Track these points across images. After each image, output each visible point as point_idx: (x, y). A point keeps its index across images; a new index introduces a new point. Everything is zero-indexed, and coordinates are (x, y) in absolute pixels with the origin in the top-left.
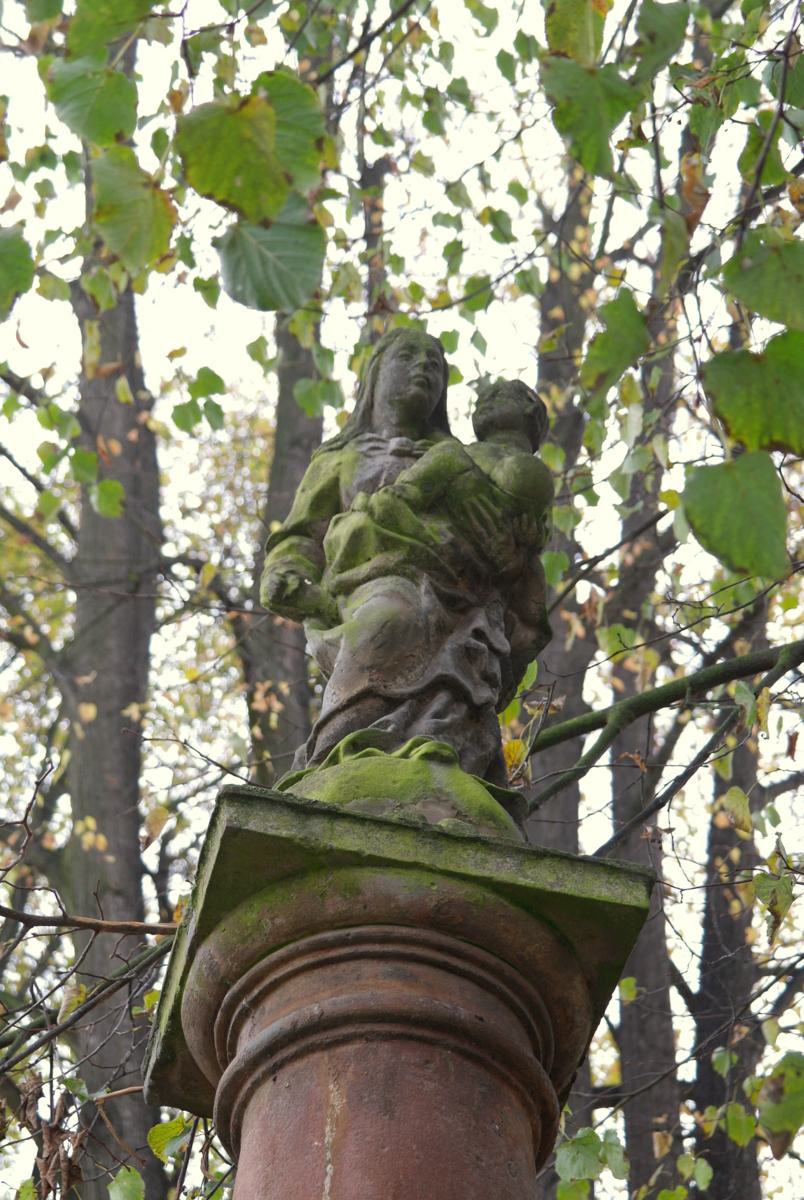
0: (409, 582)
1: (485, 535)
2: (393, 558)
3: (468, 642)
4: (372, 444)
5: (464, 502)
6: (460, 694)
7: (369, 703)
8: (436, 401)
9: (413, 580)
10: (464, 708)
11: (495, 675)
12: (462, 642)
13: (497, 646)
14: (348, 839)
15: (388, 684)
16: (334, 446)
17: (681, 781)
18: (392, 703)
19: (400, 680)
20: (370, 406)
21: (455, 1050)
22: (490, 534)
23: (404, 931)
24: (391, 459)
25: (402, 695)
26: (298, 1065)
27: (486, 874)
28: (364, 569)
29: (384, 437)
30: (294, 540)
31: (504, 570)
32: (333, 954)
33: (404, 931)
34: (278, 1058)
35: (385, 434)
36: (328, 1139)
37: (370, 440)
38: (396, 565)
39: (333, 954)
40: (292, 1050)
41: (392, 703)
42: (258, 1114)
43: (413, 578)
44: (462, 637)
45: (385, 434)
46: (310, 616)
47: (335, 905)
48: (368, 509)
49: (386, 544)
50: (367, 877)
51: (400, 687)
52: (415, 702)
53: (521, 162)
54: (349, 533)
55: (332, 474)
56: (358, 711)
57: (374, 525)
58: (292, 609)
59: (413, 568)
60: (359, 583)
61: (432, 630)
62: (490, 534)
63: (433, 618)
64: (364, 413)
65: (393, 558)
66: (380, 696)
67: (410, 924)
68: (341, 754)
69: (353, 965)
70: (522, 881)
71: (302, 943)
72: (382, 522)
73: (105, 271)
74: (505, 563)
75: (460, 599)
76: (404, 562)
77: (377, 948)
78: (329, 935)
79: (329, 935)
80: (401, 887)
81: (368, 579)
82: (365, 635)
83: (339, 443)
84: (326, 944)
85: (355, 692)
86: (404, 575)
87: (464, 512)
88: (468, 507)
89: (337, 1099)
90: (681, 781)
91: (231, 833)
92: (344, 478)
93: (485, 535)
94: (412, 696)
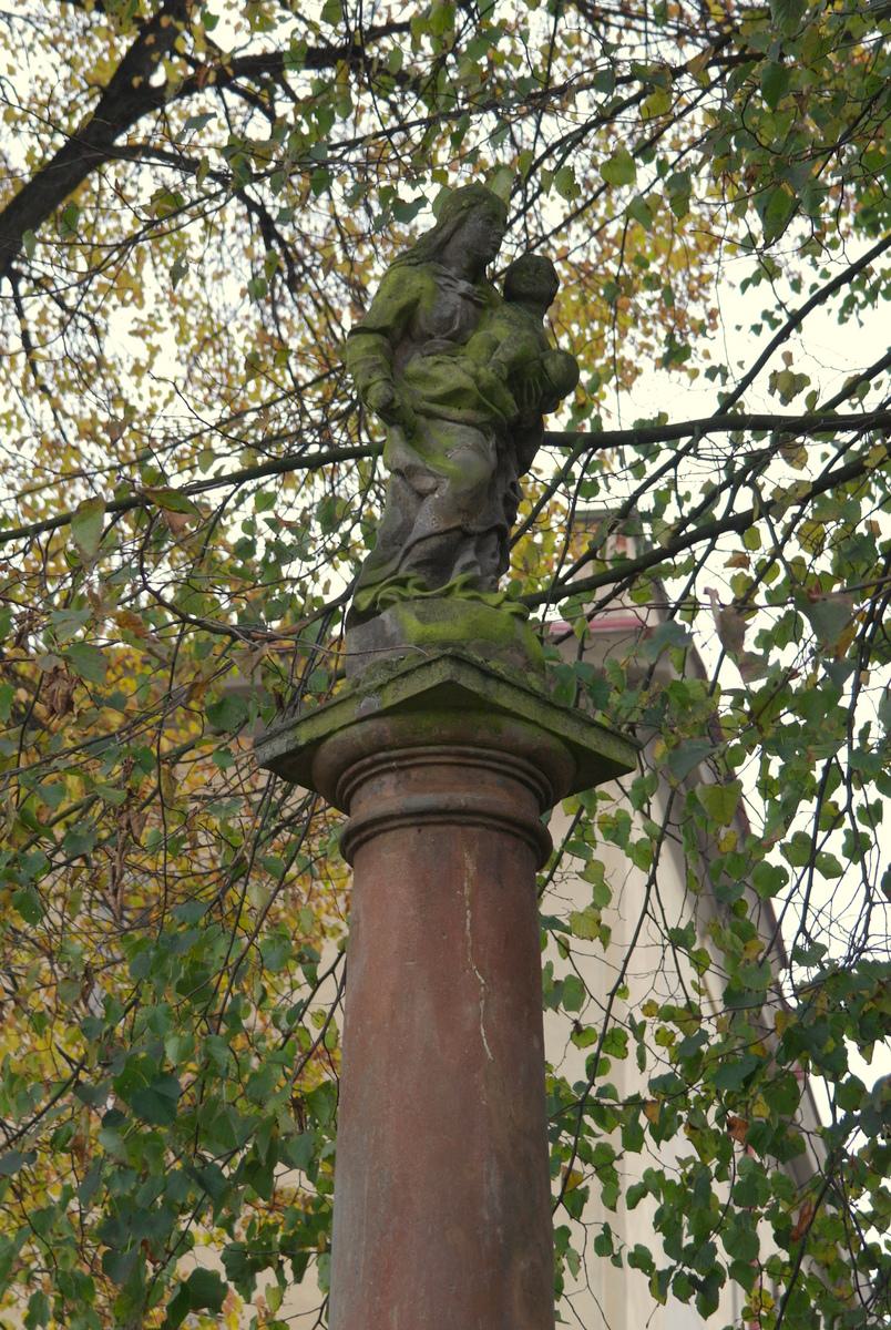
2: (481, 417)
14: (505, 699)
20: (447, 241)
21: (529, 844)
23: (513, 759)
26: (440, 829)
27: (566, 734)
28: (455, 413)
32: (471, 761)
33: (513, 759)
34: (426, 819)
36: (467, 892)
39: (471, 761)
40: (439, 819)
42: (257, 745)
43: (486, 434)
45: (452, 272)
47: (484, 734)
49: (479, 407)
50: (509, 726)
55: (415, 296)
65: (481, 417)
67: (515, 753)
69: (479, 772)
70: (583, 742)
71: (454, 749)
72: (482, 390)
73: (429, 207)
77: (496, 765)
78: (472, 750)
79: (472, 750)
80: (524, 735)
82: (466, 487)
84: (467, 756)
89: (471, 867)
92: (425, 304)
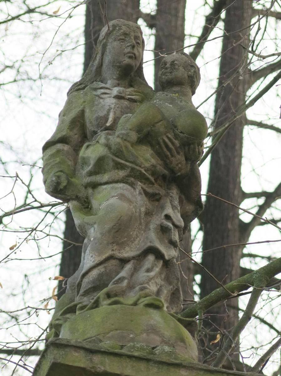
0: (129, 187)
1: (170, 156)
3: (162, 223)
4: (103, 91)
5: (159, 139)
6: (159, 255)
7: (113, 262)
8: (138, 65)
9: (132, 186)
10: (161, 262)
11: (177, 241)
12: (158, 223)
13: (177, 223)
15: (121, 251)
16: (80, 87)
17: (207, 31)
18: (124, 261)
19: (127, 249)
22: (172, 156)
24: (114, 101)
25: (129, 258)
28: (106, 177)
29: (108, 86)
30: (59, 146)
31: (179, 174)
35: (109, 84)
37: (101, 88)
38: (123, 178)
41: (124, 261)
43: (132, 185)
44: (158, 220)
46: (73, 199)
48: (108, 146)
51: (127, 253)
52: (135, 261)
53: (253, 173)
54: (97, 159)
56: (105, 267)
57: (111, 156)
58: (63, 196)
59: (132, 179)
60: (101, 184)
61: (143, 215)
62: (172, 156)
63: (143, 209)
64: (97, 68)
66: (117, 259)
68: (101, 299)
74: (180, 169)
75: (156, 194)
76: (128, 176)
81: (106, 183)
83: (83, 86)
85: (104, 257)
86: (126, 183)
87: (159, 144)
88: (161, 141)
90: (207, 31)
91: (55, 366)
93: (170, 156)
94: (133, 258)
